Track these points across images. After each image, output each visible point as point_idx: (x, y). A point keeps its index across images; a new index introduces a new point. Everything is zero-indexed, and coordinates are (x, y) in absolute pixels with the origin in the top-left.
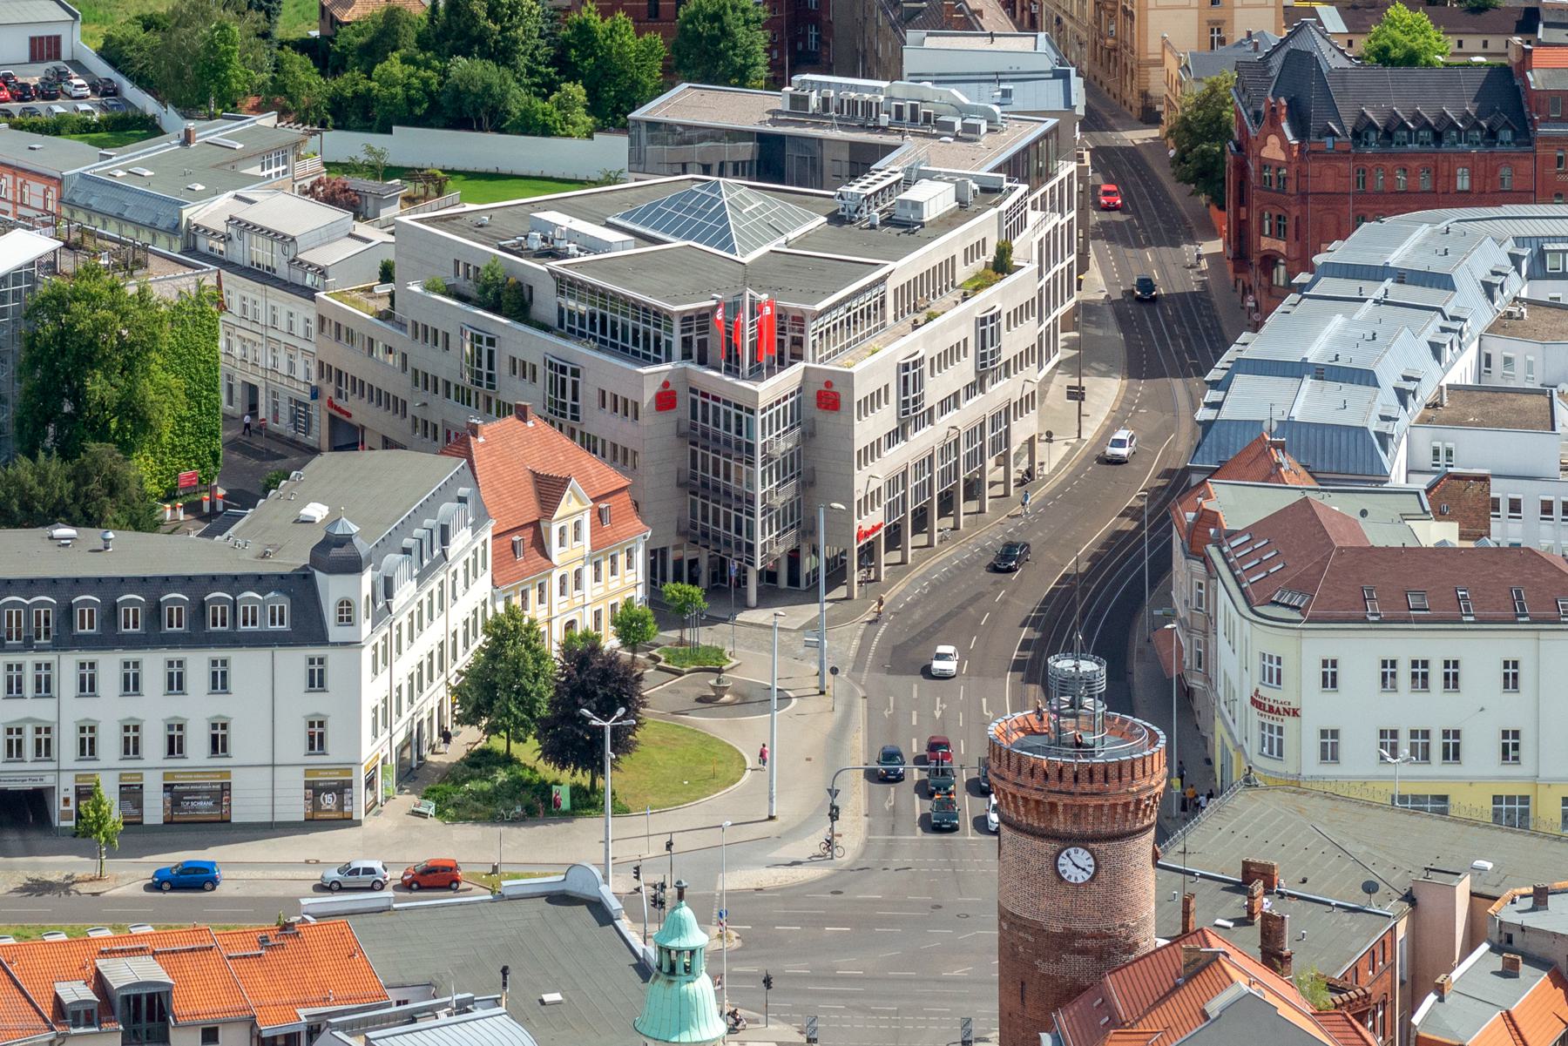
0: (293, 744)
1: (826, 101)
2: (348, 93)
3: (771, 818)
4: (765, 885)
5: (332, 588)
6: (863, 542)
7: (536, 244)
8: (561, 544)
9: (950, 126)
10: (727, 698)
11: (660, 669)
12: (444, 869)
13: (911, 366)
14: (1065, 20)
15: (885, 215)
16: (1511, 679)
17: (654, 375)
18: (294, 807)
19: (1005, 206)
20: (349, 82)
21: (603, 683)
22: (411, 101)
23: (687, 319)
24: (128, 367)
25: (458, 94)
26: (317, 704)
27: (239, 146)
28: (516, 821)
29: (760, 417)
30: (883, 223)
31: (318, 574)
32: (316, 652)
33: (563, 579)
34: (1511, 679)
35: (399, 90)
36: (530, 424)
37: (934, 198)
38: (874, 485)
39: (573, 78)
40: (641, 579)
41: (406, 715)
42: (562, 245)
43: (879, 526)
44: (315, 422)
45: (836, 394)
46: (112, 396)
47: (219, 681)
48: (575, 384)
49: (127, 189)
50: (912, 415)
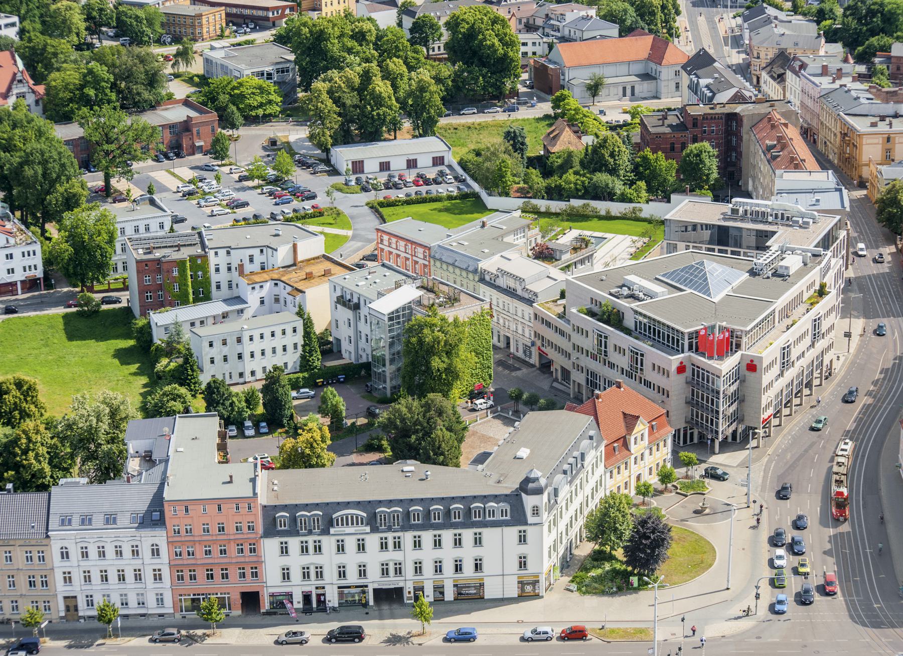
0: (512, 566)
1: (746, 211)
2: (553, 185)
3: (728, 589)
4: (725, 634)
5: (529, 501)
7: (625, 291)
8: (635, 443)
9: (797, 222)
10: (707, 511)
11: (677, 493)
12: (580, 631)
14: (828, 143)
15: (773, 271)
17: (675, 360)
18: (514, 592)
19: (823, 265)
20: (554, 181)
21: (653, 533)
22: (577, 190)
23: (690, 334)
24: (448, 353)
25: (596, 187)
26: (522, 549)
27: (504, 228)
28: (613, 594)
30: (773, 275)
31: (523, 495)
32: (522, 528)
33: (636, 458)
35: (572, 185)
37: (793, 263)
39: (640, 179)
40: (670, 451)
41: (564, 542)
42: (637, 293)
44: (533, 353)
46: (442, 366)
47: (478, 541)
48: (642, 360)
49: (456, 252)
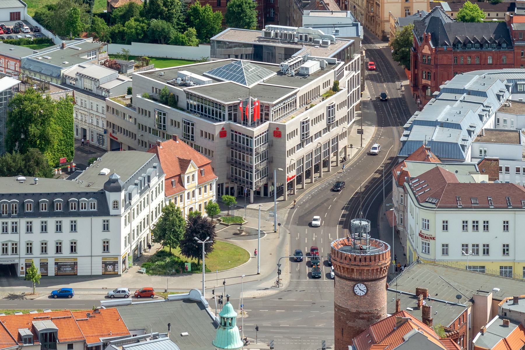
0: (98, 249)
1: (276, 34)
2: (117, 31)
3: (258, 274)
4: (256, 296)
5: (111, 197)
6: (289, 182)
7: (179, 82)
8: (188, 182)
9: (318, 42)
10: (243, 233)
11: (221, 224)
12: (149, 291)
13: (305, 123)
14: (357, 7)
15: (296, 72)
16: (506, 227)
17: (219, 125)
18: (99, 270)
19: (336, 69)
20: (117, 27)
21: (202, 229)
22: (137, 34)
23: (230, 107)
24: (43, 123)
25: (153, 32)
26: (106, 235)
27: (80, 49)
28: (173, 275)
29: (254, 139)
30: (296, 75)
31: (106, 192)
32: (106, 218)
33: (188, 194)
34: (506, 227)
35: (133, 30)
36: (178, 142)
37: (313, 66)
38: (293, 162)
39: (192, 26)
40: (215, 194)
41: (136, 239)
42: (188, 82)
43: (294, 176)
44: (105, 141)
45: (280, 132)
46: (37, 132)
47: (73, 228)
48: (193, 129)
49: (43, 63)
50: (305, 139)
